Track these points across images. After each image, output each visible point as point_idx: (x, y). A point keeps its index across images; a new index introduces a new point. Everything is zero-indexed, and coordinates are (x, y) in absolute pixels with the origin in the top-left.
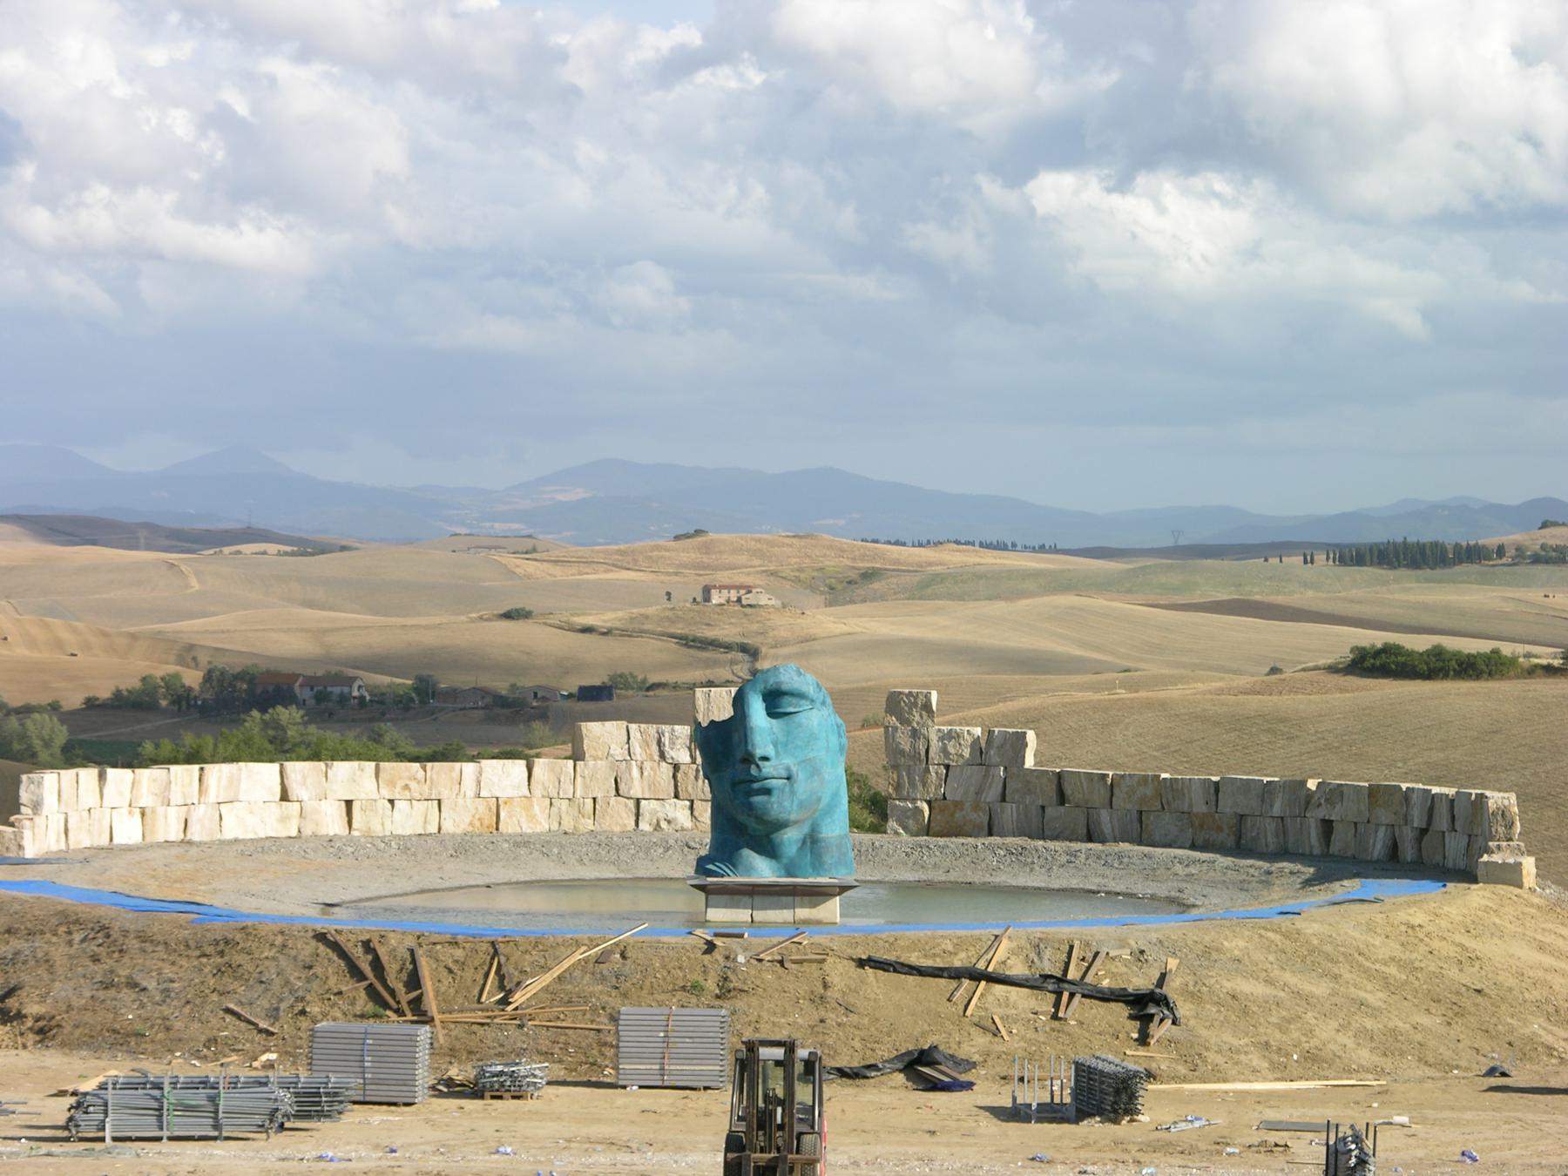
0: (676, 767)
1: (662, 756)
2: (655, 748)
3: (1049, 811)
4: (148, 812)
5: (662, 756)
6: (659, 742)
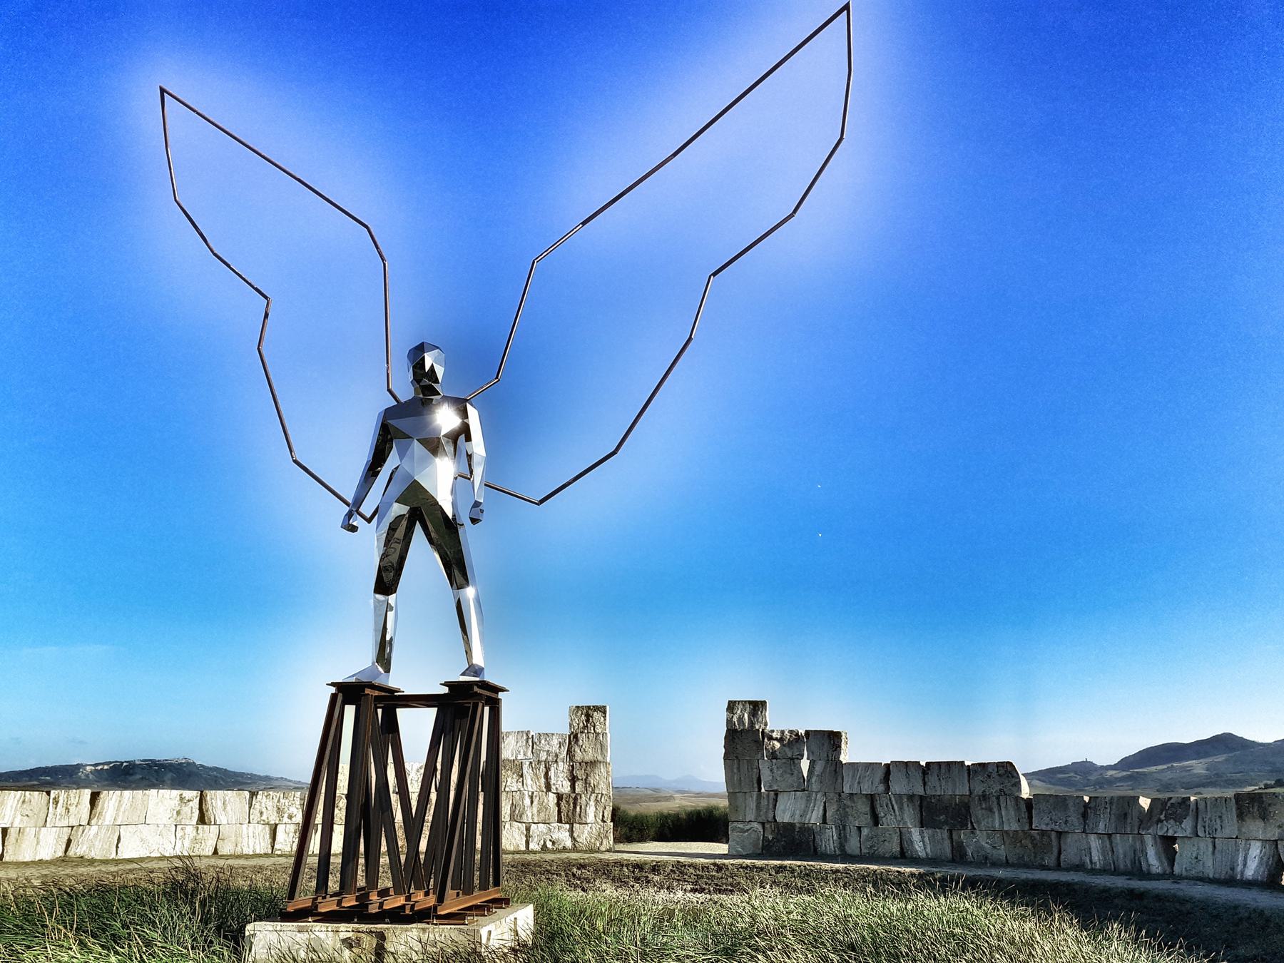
0: (560, 797)
1: (548, 788)
2: (543, 780)
3: (865, 832)
4: (12, 833)
5: (548, 788)
6: (546, 775)
